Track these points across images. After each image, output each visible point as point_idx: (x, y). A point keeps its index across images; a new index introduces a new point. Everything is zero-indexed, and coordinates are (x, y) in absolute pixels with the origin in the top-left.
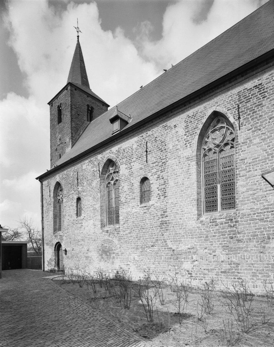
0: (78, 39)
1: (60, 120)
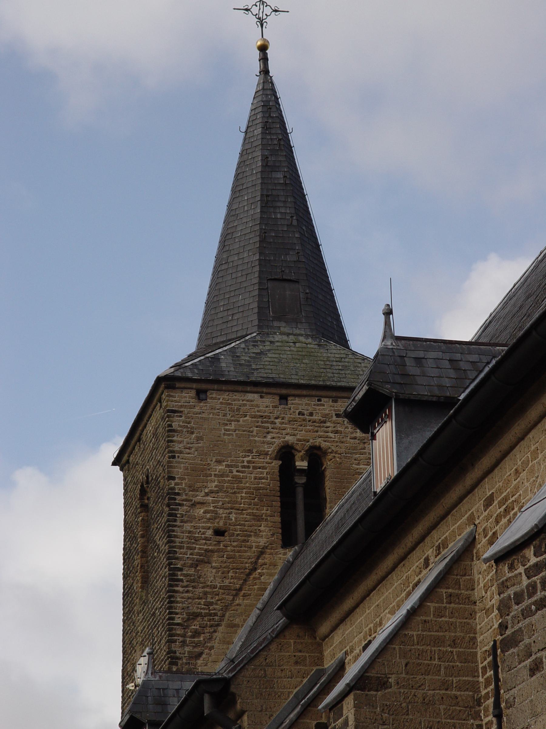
0: (264, 59)
1: (146, 581)
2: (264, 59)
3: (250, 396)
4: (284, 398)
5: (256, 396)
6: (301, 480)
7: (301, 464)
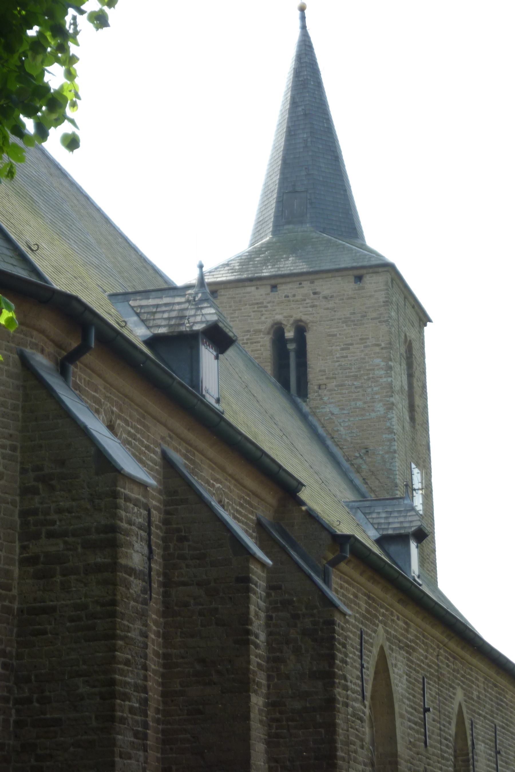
0: (303, 18)
2: (303, 18)
3: (249, 289)
4: (274, 287)
5: (253, 289)
6: (291, 347)
7: (289, 334)
